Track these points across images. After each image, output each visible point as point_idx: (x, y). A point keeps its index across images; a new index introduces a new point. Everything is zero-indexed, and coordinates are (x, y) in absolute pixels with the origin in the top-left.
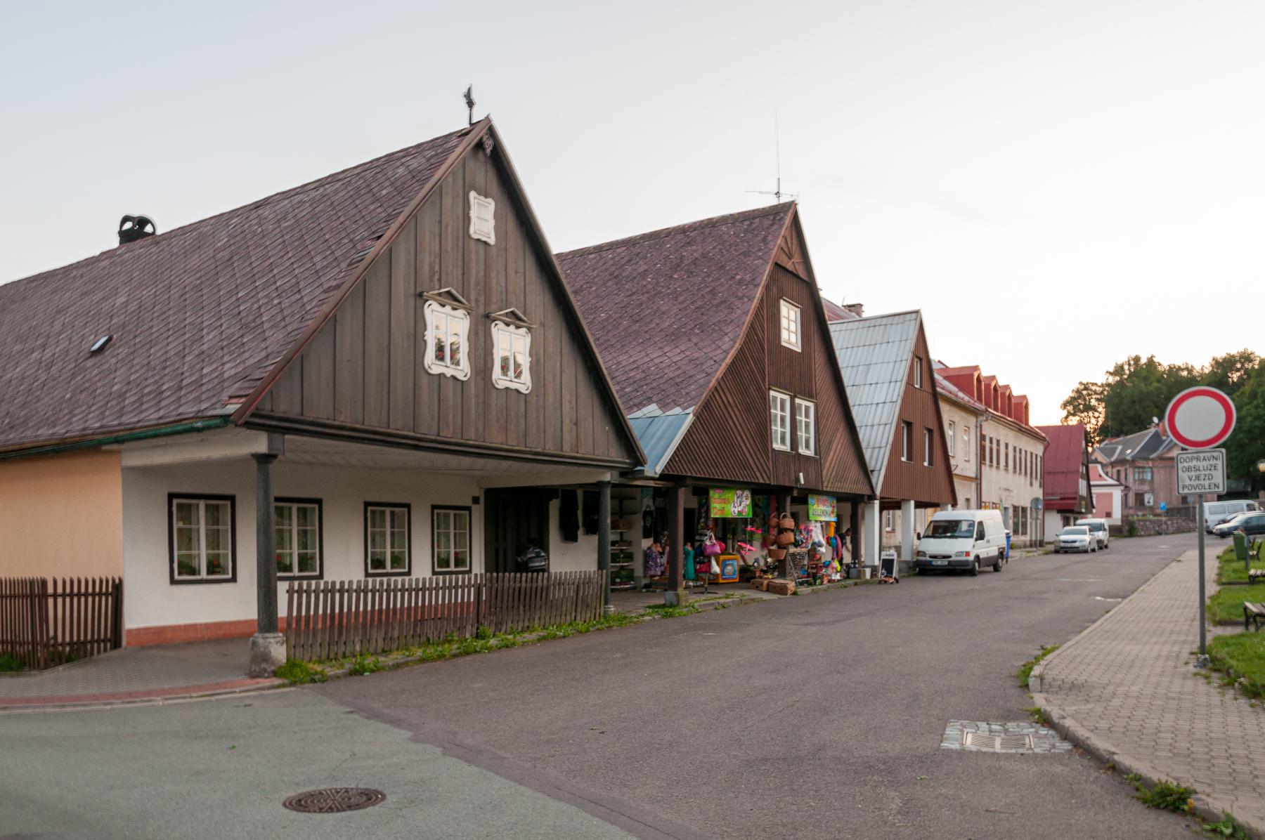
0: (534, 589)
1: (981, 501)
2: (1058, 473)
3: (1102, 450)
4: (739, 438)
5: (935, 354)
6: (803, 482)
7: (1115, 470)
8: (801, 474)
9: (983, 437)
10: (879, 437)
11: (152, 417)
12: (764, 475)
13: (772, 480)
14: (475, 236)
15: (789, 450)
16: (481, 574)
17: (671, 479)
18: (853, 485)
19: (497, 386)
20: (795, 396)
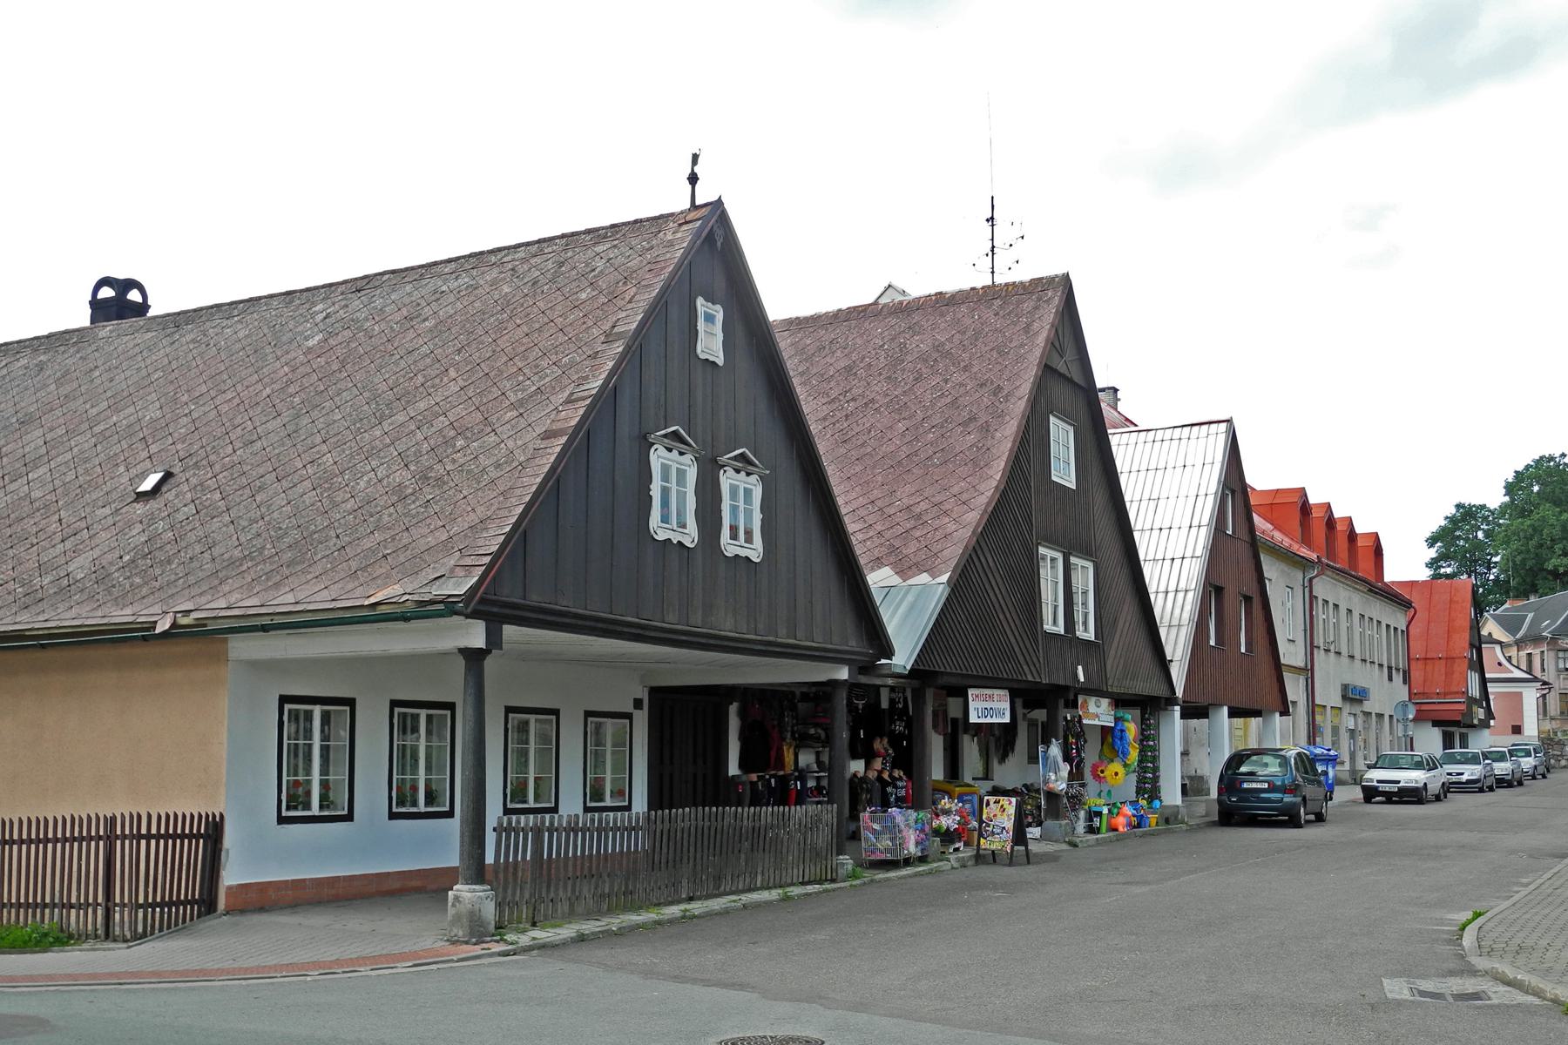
0: (757, 829)
1: (1314, 705)
2: (1429, 659)
3: (1501, 621)
4: (1001, 617)
5: (1250, 479)
6: (1082, 679)
7: (1523, 653)
8: (1080, 668)
9: (1313, 598)
10: (1177, 611)
11: (318, 597)
12: (1032, 668)
13: (1043, 676)
14: (703, 356)
15: (1093, 639)
16: (643, 813)
17: (920, 674)
18: (1148, 686)
19: (655, 536)
20: (1070, 554)
